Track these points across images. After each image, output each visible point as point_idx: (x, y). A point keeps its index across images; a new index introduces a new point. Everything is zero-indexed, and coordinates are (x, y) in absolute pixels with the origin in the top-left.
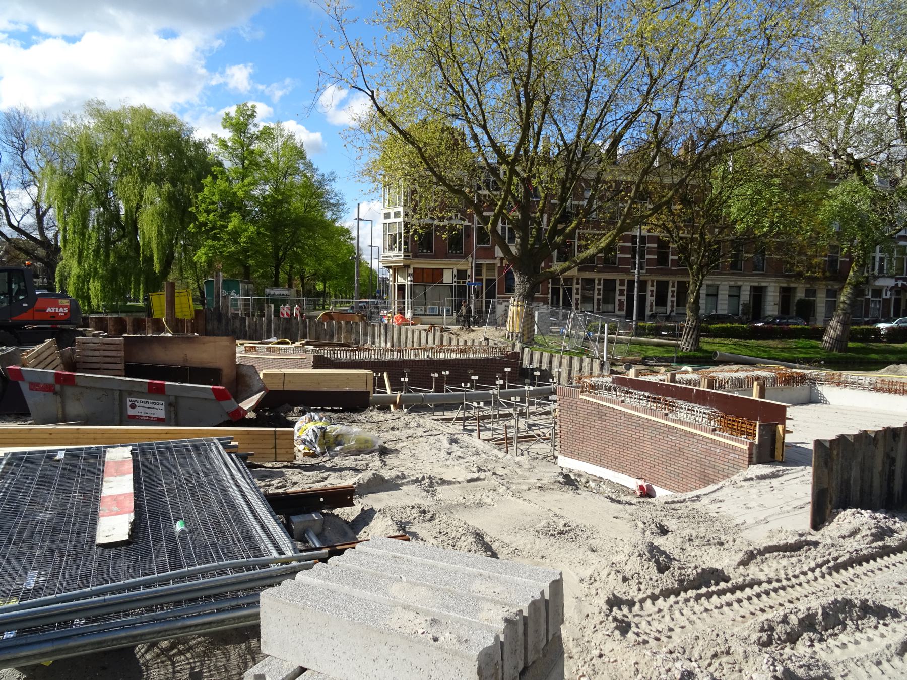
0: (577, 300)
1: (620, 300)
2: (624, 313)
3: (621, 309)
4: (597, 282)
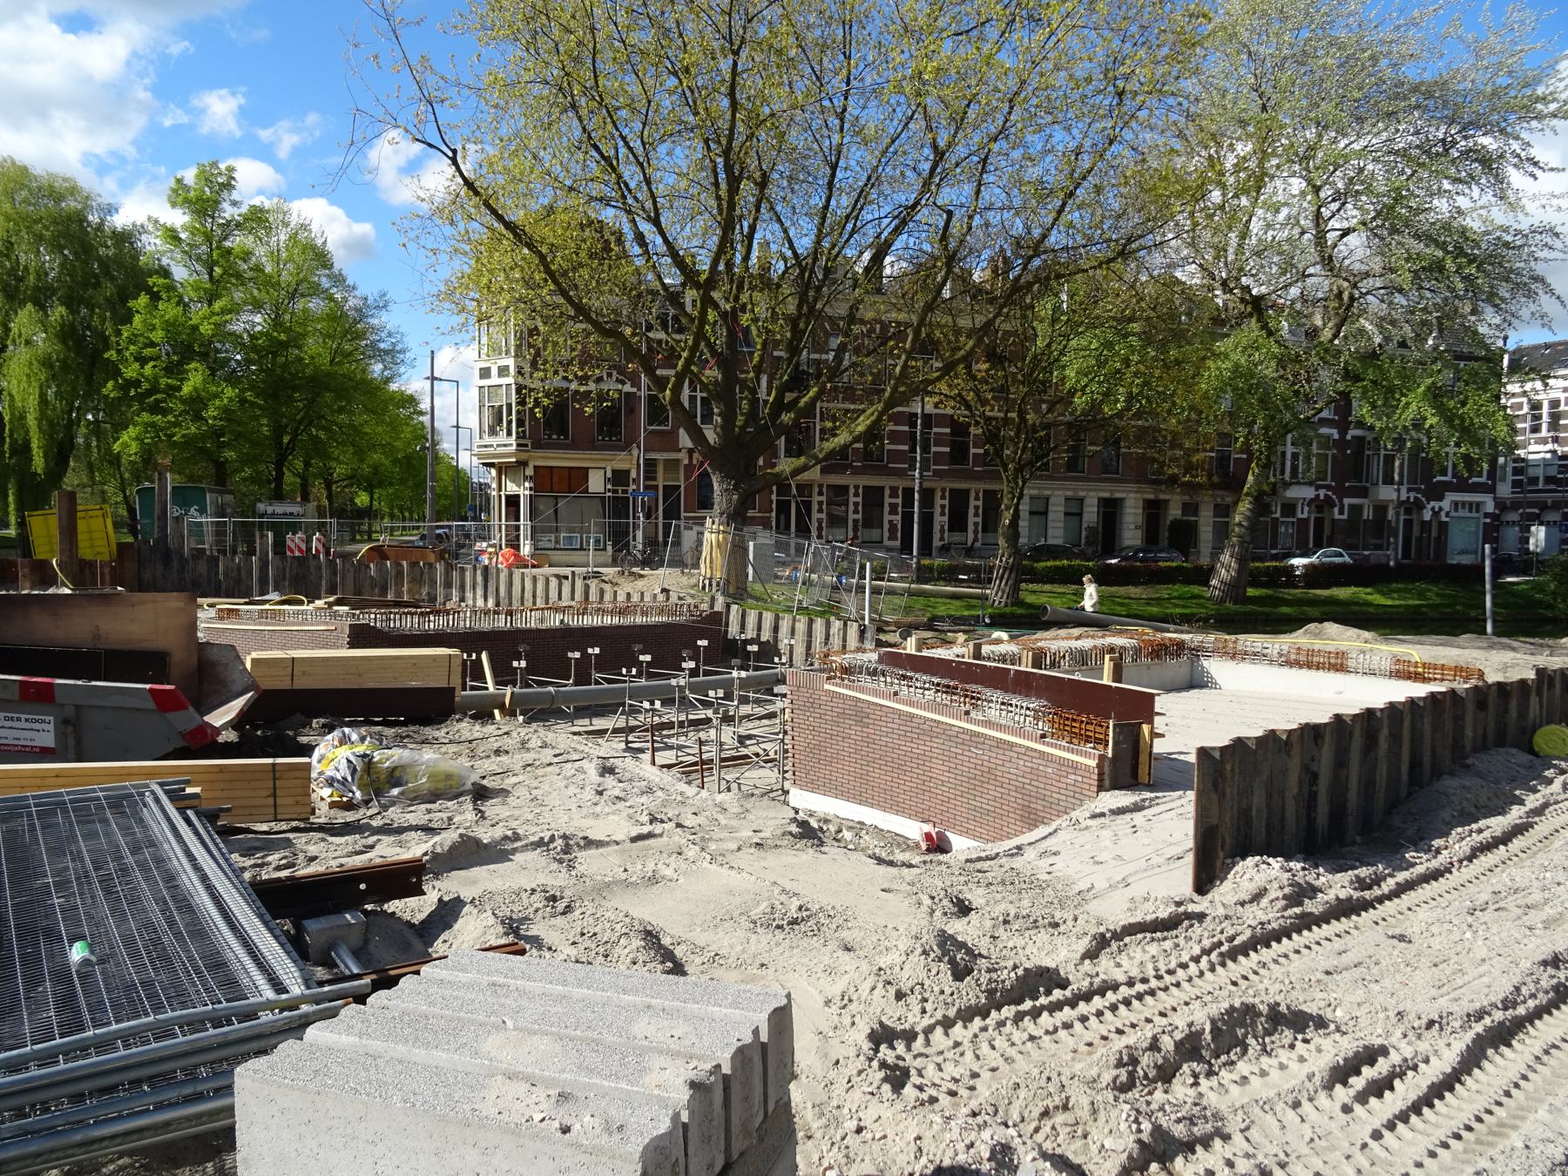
0: (820, 521)
2: (898, 543)
3: (892, 537)
4: (852, 491)
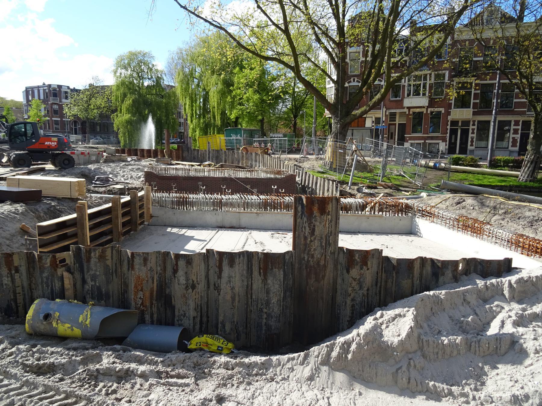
0: (472, 138)
1: (513, 138)
2: (517, 149)
3: (514, 145)
4: (471, 123)
